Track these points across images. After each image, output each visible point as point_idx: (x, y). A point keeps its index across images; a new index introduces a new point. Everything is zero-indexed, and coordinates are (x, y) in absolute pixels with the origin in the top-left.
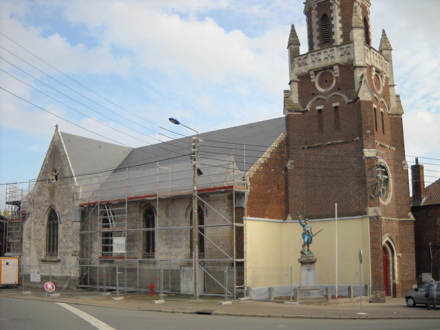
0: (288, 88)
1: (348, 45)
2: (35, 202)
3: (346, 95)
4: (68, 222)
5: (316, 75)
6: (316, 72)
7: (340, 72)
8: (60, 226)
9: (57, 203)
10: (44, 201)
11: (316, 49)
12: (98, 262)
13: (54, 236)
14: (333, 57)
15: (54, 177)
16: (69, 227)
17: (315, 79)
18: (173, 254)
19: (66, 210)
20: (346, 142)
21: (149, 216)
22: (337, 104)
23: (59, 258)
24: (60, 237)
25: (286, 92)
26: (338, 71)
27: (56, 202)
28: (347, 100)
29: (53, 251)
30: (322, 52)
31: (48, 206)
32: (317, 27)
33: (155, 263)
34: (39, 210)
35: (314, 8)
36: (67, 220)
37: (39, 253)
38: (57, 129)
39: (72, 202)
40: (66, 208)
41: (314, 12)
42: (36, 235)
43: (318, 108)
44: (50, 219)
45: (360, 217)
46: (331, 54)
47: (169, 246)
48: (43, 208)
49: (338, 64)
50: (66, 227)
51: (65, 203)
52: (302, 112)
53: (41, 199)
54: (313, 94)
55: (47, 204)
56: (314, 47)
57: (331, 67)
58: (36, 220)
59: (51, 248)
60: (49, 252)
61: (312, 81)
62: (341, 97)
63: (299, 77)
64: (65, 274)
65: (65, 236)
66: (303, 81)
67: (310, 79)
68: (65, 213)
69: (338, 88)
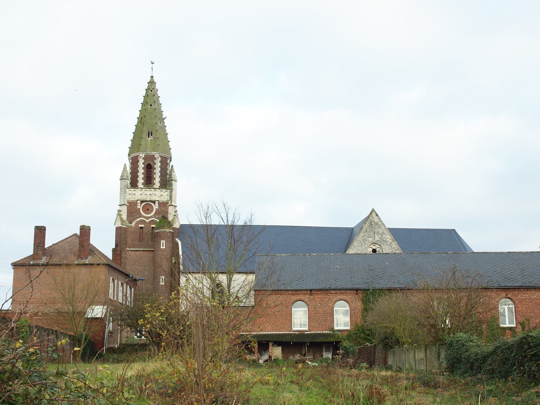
0: (119, 208)
6: (142, 202)
17: (140, 207)
43: (140, 226)
57: (154, 202)
63: (128, 202)
66: (132, 209)
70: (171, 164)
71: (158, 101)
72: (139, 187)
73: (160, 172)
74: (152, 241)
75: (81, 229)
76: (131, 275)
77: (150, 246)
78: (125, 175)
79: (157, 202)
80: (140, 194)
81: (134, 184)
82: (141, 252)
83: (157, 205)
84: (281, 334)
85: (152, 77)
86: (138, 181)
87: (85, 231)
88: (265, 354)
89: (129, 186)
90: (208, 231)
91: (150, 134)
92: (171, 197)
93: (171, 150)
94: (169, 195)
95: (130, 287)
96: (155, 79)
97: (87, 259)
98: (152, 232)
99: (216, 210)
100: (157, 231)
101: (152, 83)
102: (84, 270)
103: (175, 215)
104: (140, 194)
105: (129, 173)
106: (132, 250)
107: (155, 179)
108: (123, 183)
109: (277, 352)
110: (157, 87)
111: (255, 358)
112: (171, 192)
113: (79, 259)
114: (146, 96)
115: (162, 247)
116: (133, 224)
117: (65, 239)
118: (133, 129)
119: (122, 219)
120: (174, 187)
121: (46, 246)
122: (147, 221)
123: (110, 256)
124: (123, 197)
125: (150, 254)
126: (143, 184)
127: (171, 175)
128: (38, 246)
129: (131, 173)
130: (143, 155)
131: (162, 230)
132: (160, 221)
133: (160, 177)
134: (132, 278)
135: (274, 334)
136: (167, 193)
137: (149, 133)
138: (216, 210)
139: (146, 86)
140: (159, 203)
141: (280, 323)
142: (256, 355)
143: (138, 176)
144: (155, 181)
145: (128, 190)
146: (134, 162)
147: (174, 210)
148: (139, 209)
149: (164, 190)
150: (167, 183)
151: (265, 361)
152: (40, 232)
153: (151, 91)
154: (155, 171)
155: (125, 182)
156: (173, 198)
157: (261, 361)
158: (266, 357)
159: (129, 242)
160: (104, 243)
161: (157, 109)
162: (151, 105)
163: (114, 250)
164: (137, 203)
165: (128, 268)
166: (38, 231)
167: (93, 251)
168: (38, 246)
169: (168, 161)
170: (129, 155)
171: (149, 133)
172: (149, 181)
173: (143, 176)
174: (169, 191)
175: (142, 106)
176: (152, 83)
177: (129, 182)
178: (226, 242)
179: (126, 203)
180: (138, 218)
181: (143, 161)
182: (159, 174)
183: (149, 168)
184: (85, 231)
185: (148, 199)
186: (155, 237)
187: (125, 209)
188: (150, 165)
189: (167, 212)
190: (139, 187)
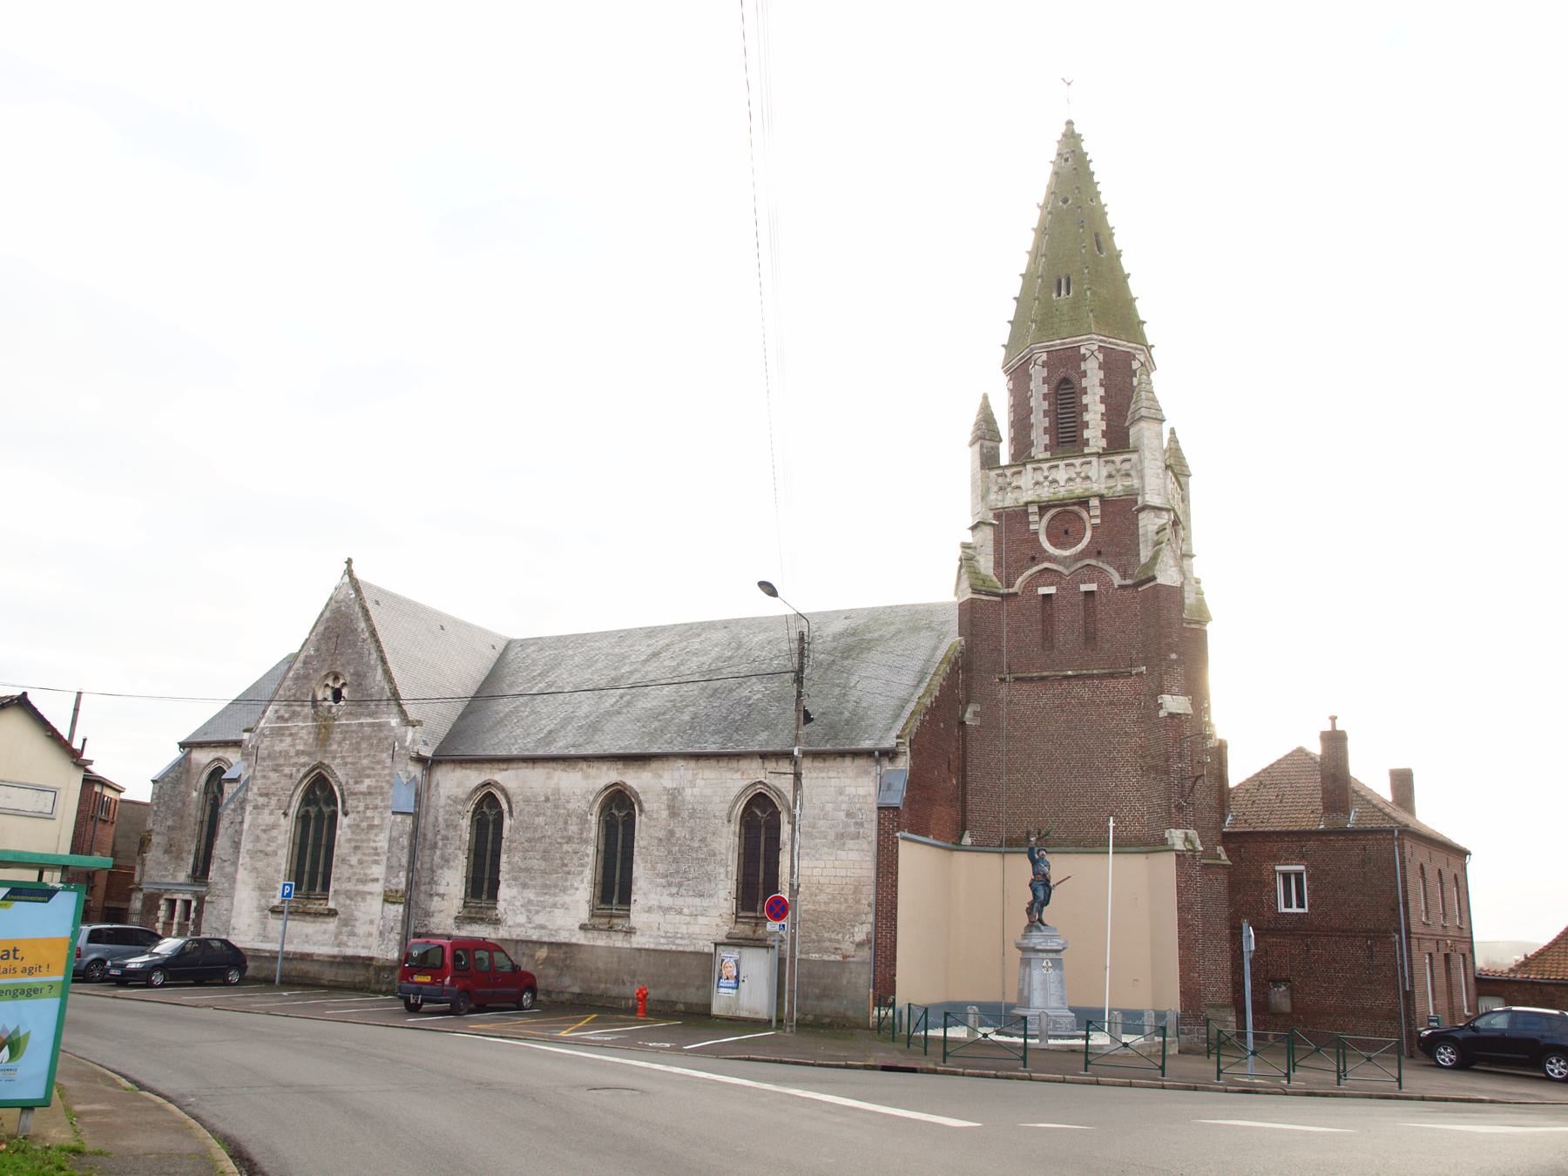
0: (968, 537)
1: (1126, 456)
2: (263, 752)
3: (1117, 569)
4: (369, 813)
5: (1041, 516)
6: (1043, 508)
7: (1103, 516)
8: (343, 821)
9: (338, 761)
10: (292, 752)
11: (1041, 456)
12: (451, 921)
13: (317, 846)
14: (1088, 478)
15: (329, 693)
16: (371, 827)
17: (1039, 525)
18: (686, 911)
19: (367, 782)
20: (1112, 675)
21: (614, 811)
22: (1093, 587)
23: (331, 905)
24: (342, 846)
25: (965, 546)
26: (1098, 512)
27: (334, 758)
28: (1117, 580)
29: (312, 886)
30: (1062, 464)
31: (304, 765)
32: (1045, 405)
33: (630, 932)
34: (274, 775)
35: (1040, 362)
36: (367, 808)
37: (263, 888)
38: (349, 572)
39: (389, 761)
40: (368, 776)
41: (1038, 373)
42: (258, 839)
43: (1043, 591)
44: (308, 799)
45: (785, 830)
46: (1085, 470)
47: (674, 890)
48: (287, 770)
49: (1101, 497)
50: (364, 825)
51: (365, 762)
52: (1002, 596)
53: (284, 745)
54: (1033, 558)
55: (303, 759)
56: (1033, 451)
57: (1083, 502)
58: (261, 800)
59: (306, 877)
60: (298, 888)
61: (1032, 527)
62: (1102, 571)
63: (997, 516)
64: (350, 952)
65: (357, 848)
66: (1008, 529)
67: (1029, 523)
68: (363, 787)
69: (1095, 551)
79: (1095, 502)
80: (1029, 487)
93: (1145, 327)
101: (985, 397)
137: (1060, 282)
154: (1086, 400)
164: (1026, 514)
176: (985, 397)
182: (1101, 392)
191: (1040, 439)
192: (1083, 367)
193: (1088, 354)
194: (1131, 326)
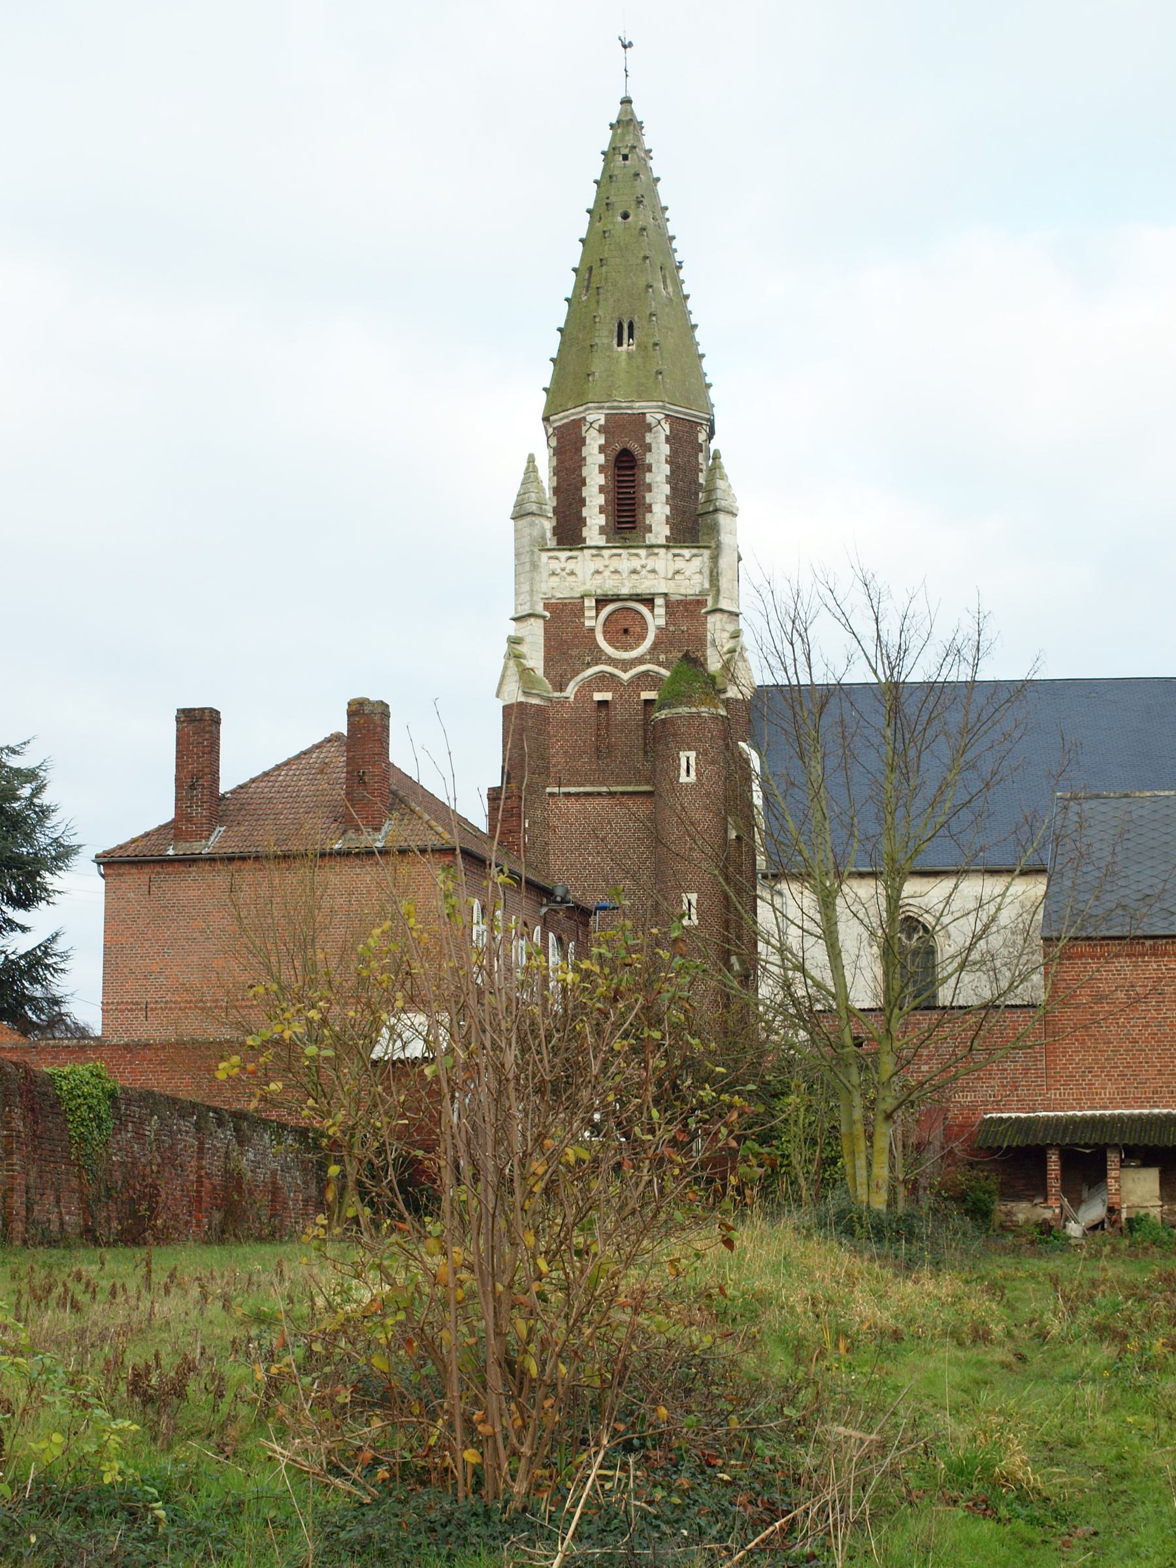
0: (512, 629)
6: (601, 602)
14: (572, 573)
17: (594, 620)
43: (598, 696)
57: (649, 601)
63: (547, 607)
66: (564, 630)
70: (713, 446)
71: (655, 195)
72: (589, 543)
73: (670, 480)
74: (663, 757)
75: (351, 714)
76: (559, 892)
77: (640, 779)
78: (533, 497)
79: (659, 601)
80: (596, 570)
81: (569, 533)
82: (605, 802)
83: (660, 611)
84: (1157, 1116)
85: (627, 101)
86: (582, 522)
87: (368, 723)
88: (1092, 1197)
89: (552, 542)
90: (902, 713)
91: (624, 330)
92: (714, 577)
94: (706, 572)
95: (559, 939)
96: (640, 112)
97: (377, 829)
98: (646, 721)
99: (831, 604)
100: (663, 715)
101: (627, 125)
102: (365, 876)
103: (732, 651)
104: (596, 570)
105: (548, 494)
106: (568, 795)
107: (649, 509)
108: (527, 531)
109: (1139, 1189)
110: (648, 141)
111: (1048, 1214)
112: (715, 559)
113: (351, 834)
114: (606, 182)
115: (683, 779)
116: (571, 691)
117: (298, 757)
118: (560, 314)
119: (525, 674)
120: (725, 538)
121: (226, 785)
122: (626, 677)
123: (477, 814)
124: (526, 587)
125: (641, 808)
126: (602, 530)
127: (711, 490)
128: (192, 787)
129: (556, 491)
130: (598, 417)
131: (683, 710)
132: (675, 674)
133: (671, 500)
134: (564, 901)
135: (1130, 1118)
136: (697, 562)
137: (620, 326)
138: (831, 604)
139: (604, 139)
140: (668, 605)
141: (1153, 1072)
142: (1052, 1202)
143: (583, 502)
144: (649, 518)
145: (544, 556)
146: (567, 446)
147: (731, 628)
148: (592, 630)
149: (687, 553)
150: (697, 522)
151: (1094, 1228)
152: (198, 731)
153: (625, 158)
154: (649, 478)
155: (532, 524)
156: (724, 583)
157: (1074, 1230)
158: (1094, 1211)
159: (558, 760)
160: (455, 761)
161: (651, 230)
162: (625, 216)
163: (494, 795)
165: (555, 863)
166: (189, 729)
167: (404, 796)
168: (192, 787)
169: (702, 437)
170: (546, 419)
171: (620, 326)
172: (626, 520)
173: (601, 500)
174: (706, 553)
175: (591, 224)
176: (627, 125)
177: (548, 525)
178: (876, 740)
179: (540, 609)
180: (589, 665)
181: (602, 441)
182: (667, 489)
183: (626, 467)
184: (368, 723)
185: (625, 591)
186: (657, 739)
187: (535, 632)
188: (629, 448)
189: (700, 641)
190: (589, 543)
191: (595, 519)
192: (648, 440)
193: (654, 422)
194: (695, 387)
